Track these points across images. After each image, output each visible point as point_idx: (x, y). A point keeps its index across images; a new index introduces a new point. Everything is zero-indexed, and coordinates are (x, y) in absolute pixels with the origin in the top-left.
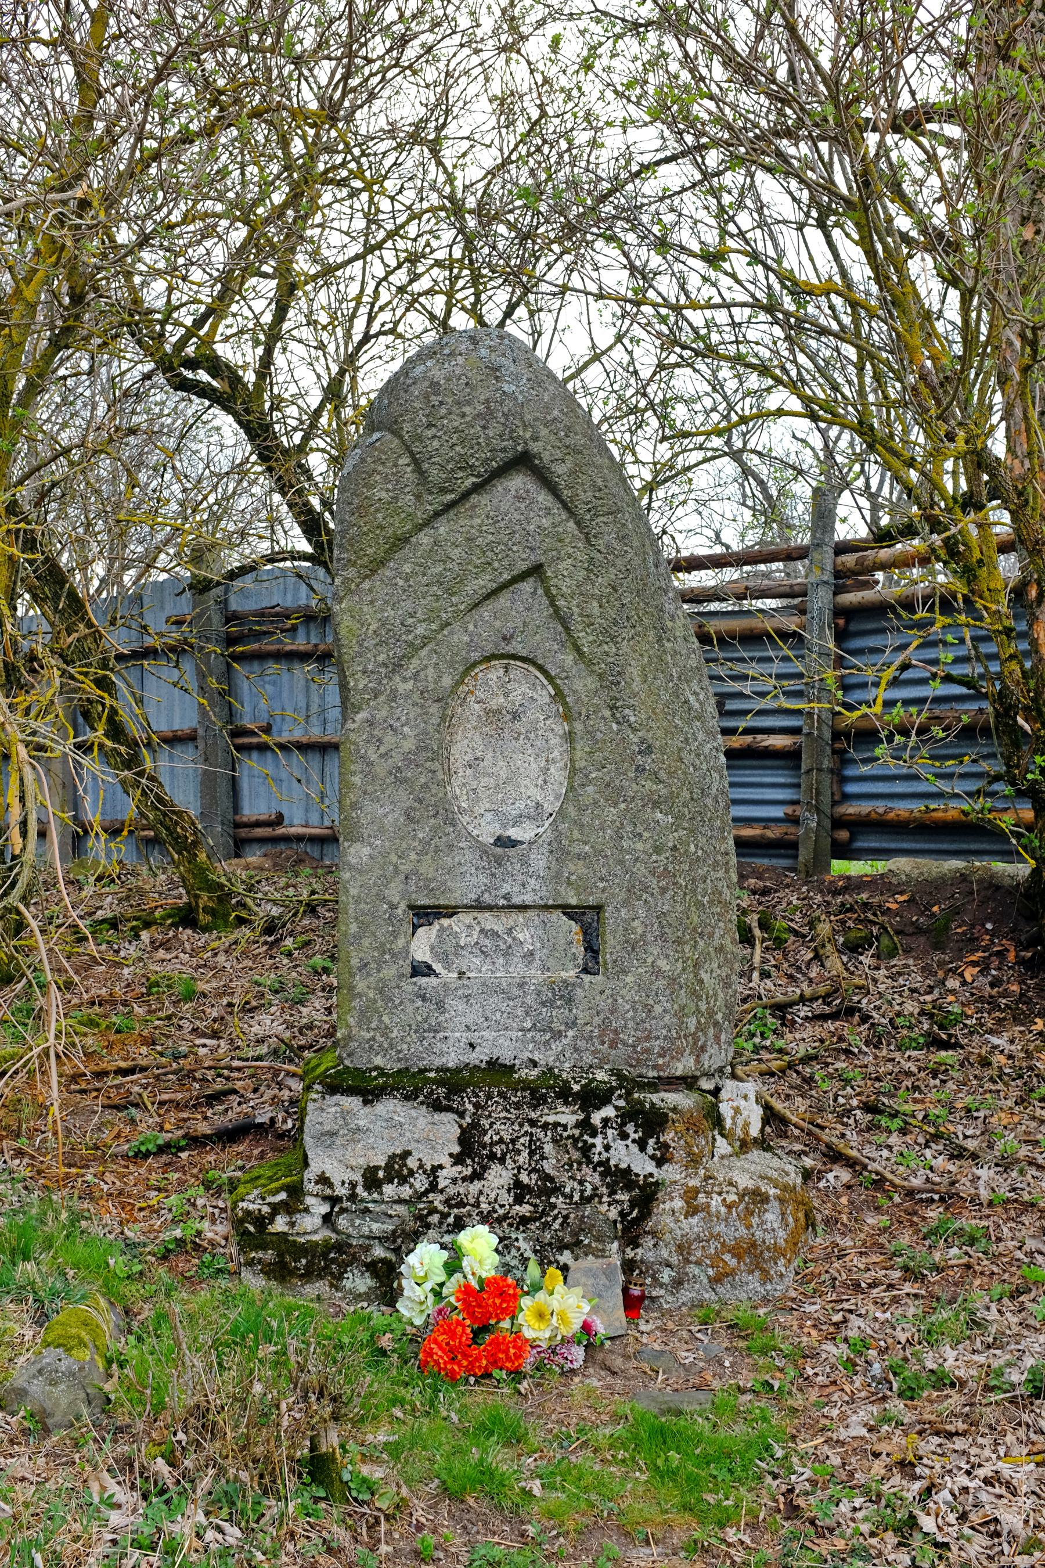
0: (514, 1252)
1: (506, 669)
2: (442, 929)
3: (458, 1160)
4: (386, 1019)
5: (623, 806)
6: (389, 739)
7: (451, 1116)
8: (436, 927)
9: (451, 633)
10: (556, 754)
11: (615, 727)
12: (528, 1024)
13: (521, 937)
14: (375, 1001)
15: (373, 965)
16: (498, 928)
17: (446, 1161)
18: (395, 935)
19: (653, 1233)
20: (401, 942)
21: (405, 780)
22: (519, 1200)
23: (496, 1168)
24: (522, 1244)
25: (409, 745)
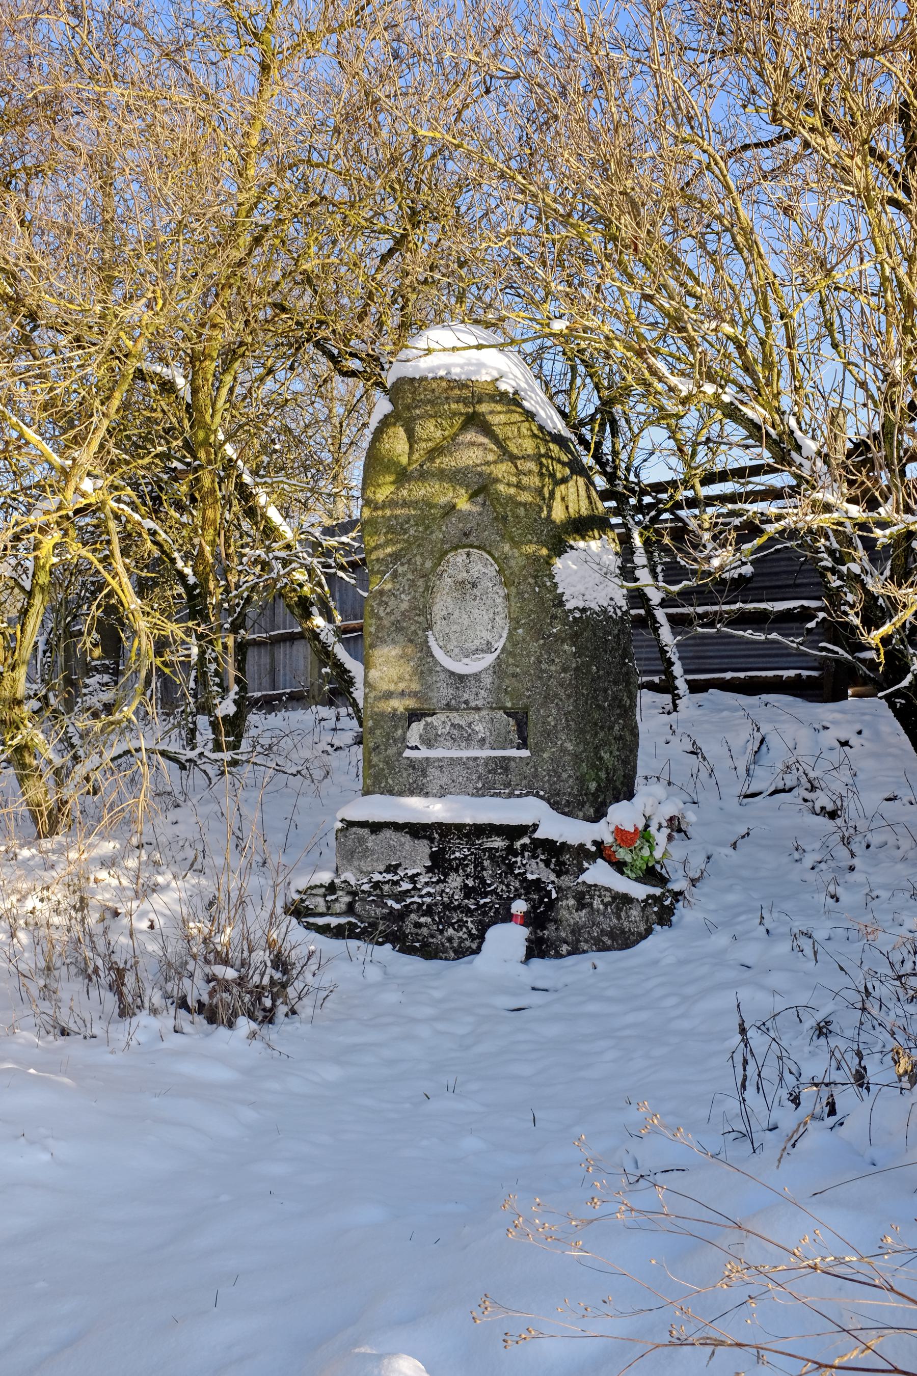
0: (464, 929)
1: (468, 555)
2: (427, 724)
3: (429, 870)
4: (390, 781)
5: (542, 642)
6: (393, 603)
7: (426, 842)
8: (423, 722)
9: (432, 533)
10: (500, 608)
11: (537, 589)
12: (480, 785)
13: (477, 728)
14: (383, 770)
15: (382, 747)
16: (462, 723)
17: (423, 870)
18: (396, 727)
19: (556, 921)
20: (400, 732)
21: (402, 629)
22: (467, 896)
23: (453, 875)
24: (470, 925)
25: (405, 606)
